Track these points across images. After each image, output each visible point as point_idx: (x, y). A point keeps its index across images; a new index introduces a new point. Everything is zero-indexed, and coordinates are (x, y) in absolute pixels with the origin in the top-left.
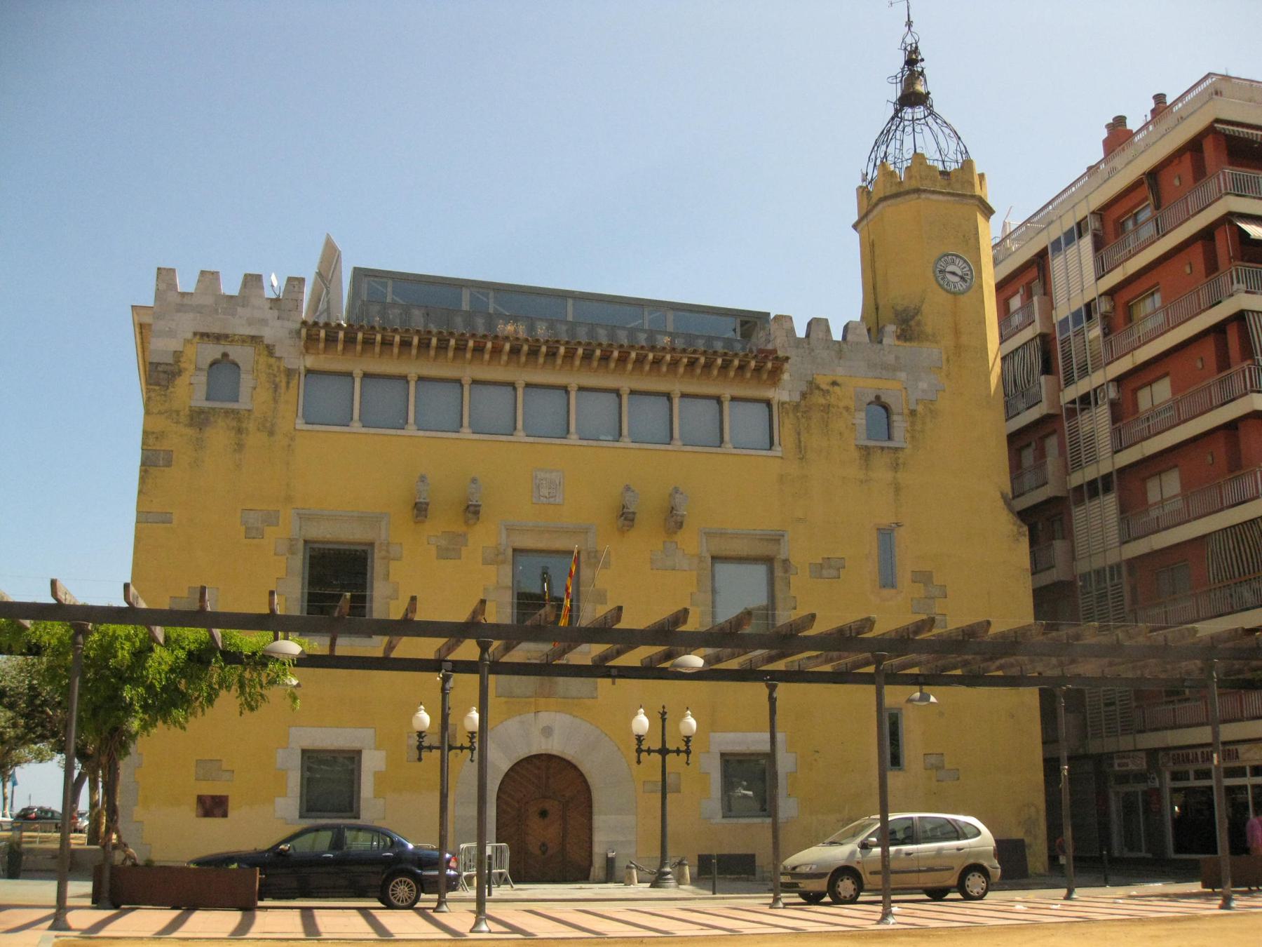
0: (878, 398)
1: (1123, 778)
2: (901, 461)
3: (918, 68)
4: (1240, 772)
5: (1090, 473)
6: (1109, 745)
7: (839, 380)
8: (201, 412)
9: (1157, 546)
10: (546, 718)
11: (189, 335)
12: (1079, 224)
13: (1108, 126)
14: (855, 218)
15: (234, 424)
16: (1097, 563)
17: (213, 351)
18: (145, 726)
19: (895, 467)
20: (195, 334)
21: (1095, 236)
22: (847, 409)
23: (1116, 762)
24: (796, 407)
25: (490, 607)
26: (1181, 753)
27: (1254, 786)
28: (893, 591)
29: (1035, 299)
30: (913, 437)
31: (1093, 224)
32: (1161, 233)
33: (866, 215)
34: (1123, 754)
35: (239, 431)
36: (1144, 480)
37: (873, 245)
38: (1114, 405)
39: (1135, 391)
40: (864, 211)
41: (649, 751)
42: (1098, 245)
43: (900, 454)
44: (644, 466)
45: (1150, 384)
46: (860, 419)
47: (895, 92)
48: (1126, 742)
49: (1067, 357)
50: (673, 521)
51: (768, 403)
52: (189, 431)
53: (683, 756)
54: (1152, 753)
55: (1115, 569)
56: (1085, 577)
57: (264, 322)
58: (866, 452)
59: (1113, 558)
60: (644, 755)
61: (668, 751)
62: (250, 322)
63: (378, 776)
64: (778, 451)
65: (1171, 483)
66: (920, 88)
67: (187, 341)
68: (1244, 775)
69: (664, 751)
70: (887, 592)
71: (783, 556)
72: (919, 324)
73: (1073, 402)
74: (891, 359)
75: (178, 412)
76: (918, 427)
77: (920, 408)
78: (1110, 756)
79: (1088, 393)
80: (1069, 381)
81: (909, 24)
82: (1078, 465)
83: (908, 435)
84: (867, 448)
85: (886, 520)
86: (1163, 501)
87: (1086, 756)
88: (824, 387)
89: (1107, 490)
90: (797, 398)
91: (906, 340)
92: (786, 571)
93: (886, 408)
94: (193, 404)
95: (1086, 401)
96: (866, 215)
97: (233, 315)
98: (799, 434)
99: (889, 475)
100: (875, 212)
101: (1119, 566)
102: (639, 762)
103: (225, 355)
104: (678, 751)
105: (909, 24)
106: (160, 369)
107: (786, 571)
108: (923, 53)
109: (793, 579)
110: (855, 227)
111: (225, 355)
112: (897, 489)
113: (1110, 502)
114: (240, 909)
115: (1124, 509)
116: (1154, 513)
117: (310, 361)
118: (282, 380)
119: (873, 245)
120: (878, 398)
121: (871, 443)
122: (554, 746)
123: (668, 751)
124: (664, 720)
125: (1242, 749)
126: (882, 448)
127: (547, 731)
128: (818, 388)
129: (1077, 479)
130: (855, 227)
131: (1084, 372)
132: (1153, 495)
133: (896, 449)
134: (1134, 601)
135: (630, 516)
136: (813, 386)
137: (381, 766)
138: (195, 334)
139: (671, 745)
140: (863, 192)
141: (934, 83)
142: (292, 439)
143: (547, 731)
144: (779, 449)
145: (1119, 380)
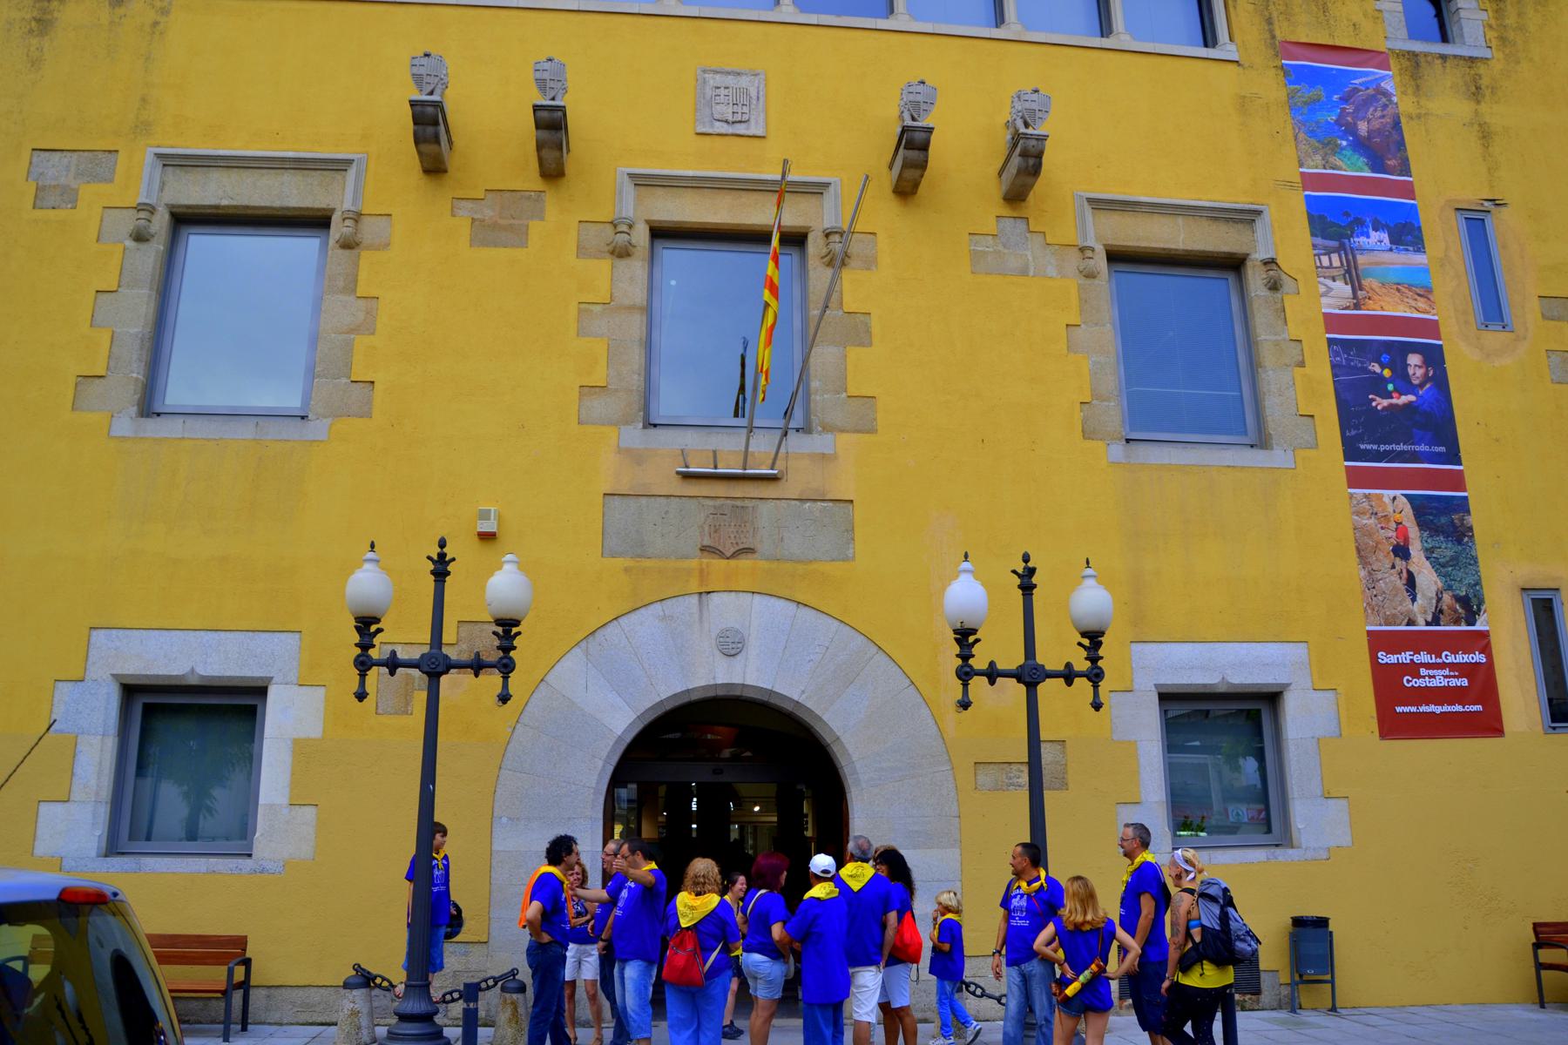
2: (1484, 82)
10: (727, 609)
18: (1128, 1007)
19: (1476, 92)
25: (695, 609)
28: (1503, 337)
30: (1502, 39)
41: (992, 674)
43: (1482, 69)
53: (1082, 684)
60: (978, 684)
63: (302, 750)
69: (1030, 676)
70: (1494, 338)
71: (1260, 254)
76: (1511, 20)
83: (1491, 34)
84: (1413, 56)
92: (1274, 286)
98: (1269, 21)
99: (1462, 108)
102: (965, 705)
104: (1069, 675)
107: (1274, 286)
109: (1290, 302)
114: (642, 959)
121: (1418, 47)
122: (752, 673)
124: (1027, 588)
126: (1444, 57)
127: (732, 646)
133: (1472, 59)
135: (919, 136)
137: (313, 728)
139: (1049, 657)
143: (732, 646)
144: (1233, 47)
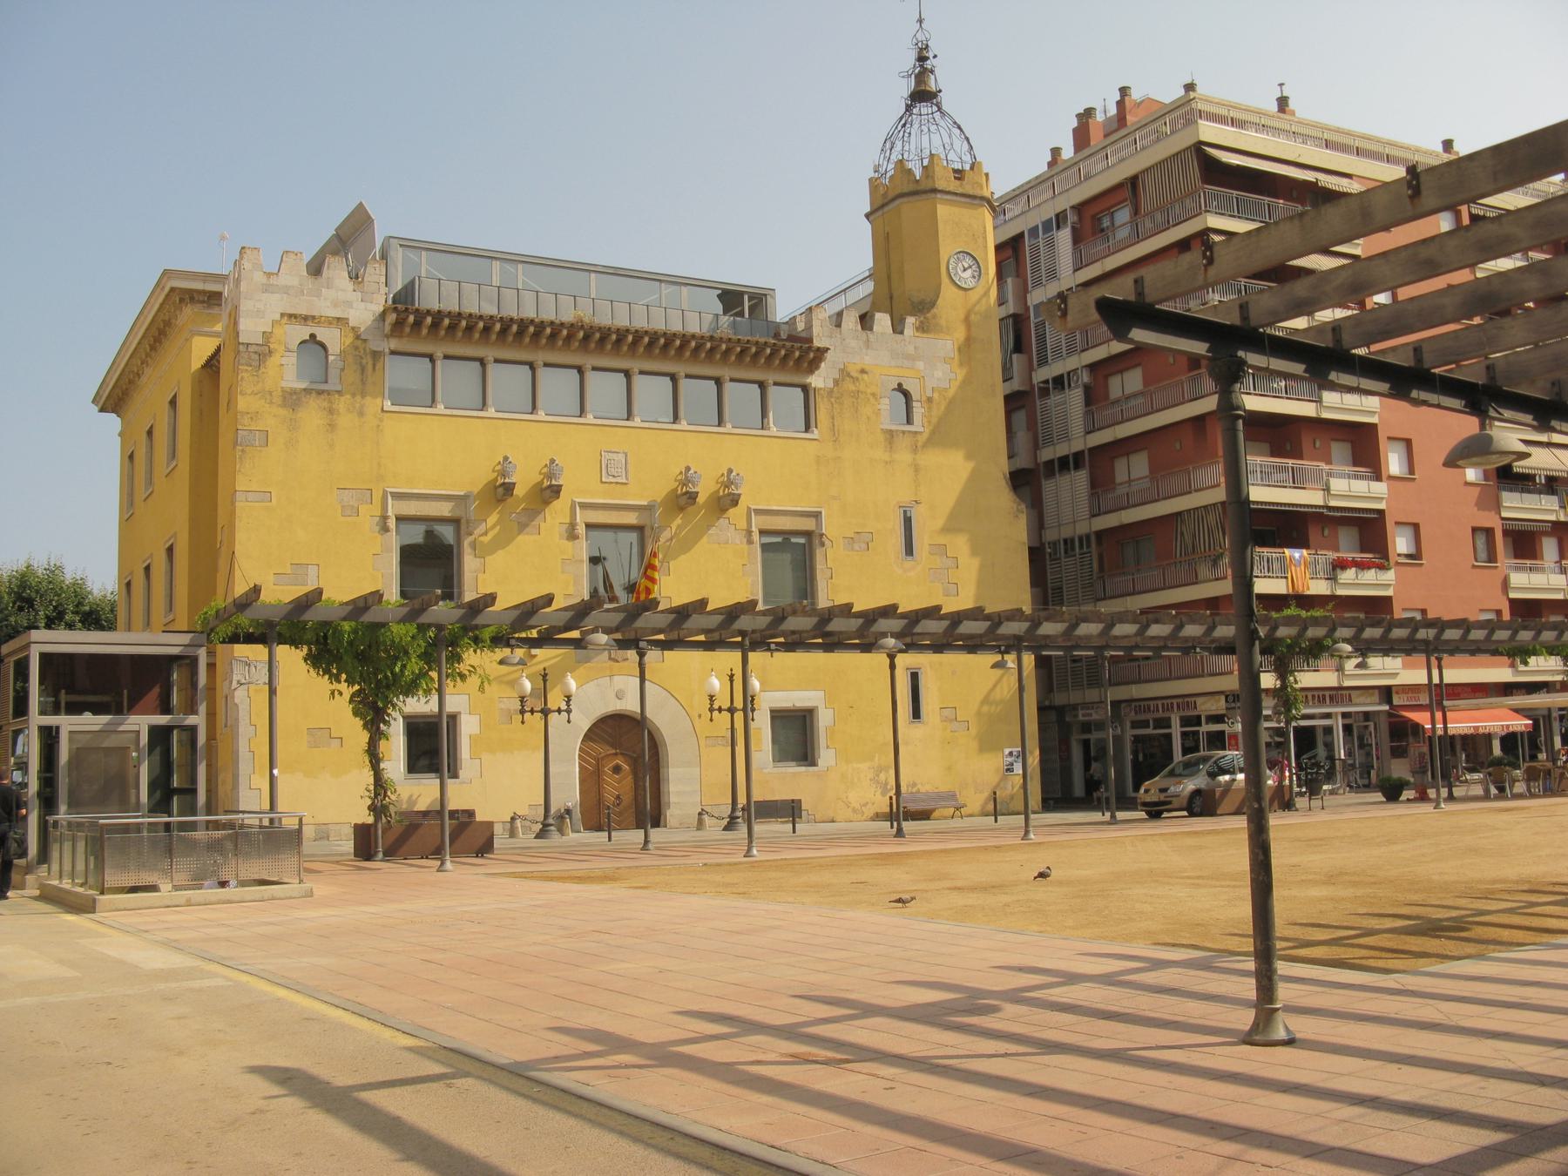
0: (900, 385)
1: (1087, 727)
3: (928, 65)
4: (1145, 724)
5: (1062, 450)
6: (1075, 697)
7: (867, 368)
8: (294, 392)
9: (1126, 521)
11: (277, 317)
12: (1057, 216)
13: (1078, 116)
14: (868, 209)
15: (325, 404)
16: (1066, 532)
17: (303, 332)
20: (282, 315)
21: (1074, 230)
22: (873, 395)
23: (1081, 712)
24: (831, 392)
26: (1186, 700)
27: (1169, 737)
29: (1009, 280)
31: (1072, 218)
32: (1138, 238)
33: (883, 206)
34: (1087, 705)
35: (331, 411)
36: (1113, 459)
37: (887, 237)
38: (1088, 390)
39: (1106, 377)
40: (879, 202)
42: (1077, 239)
44: (704, 452)
45: (1121, 372)
46: (885, 404)
47: (905, 87)
48: (1092, 695)
49: (1042, 339)
50: (726, 501)
51: (805, 389)
52: (283, 412)
54: (1116, 704)
55: (1085, 539)
56: (1054, 544)
57: (349, 304)
58: (890, 435)
59: (1082, 528)
61: (542, 711)
62: (335, 305)
64: (815, 434)
65: (1139, 465)
66: (932, 87)
67: (274, 323)
68: (1148, 726)
72: (934, 317)
73: (1046, 382)
74: (910, 349)
75: (270, 393)
77: (936, 396)
78: (1074, 707)
79: (1062, 376)
80: (1043, 361)
81: (920, 21)
82: (1049, 441)
85: (906, 497)
86: (1130, 481)
87: (1051, 708)
88: (854, 374)
89: (1077, 467)
90: (831, 384)
91: (924, 331)
93: (906, 394)
94: (284, 384)
95: (1059, 382)
96: (883, 206)
97: (319, 296)
100: (891, 206)
101: (1088, 536)
103: (313, 336)
105: (920, 21)
106: (251, 349)
108: (934, 48)
110: (867, 216)
111: (313, 336)
112: (917, 469)
113: (1081, 478)
115: (1094, 484)
116: (1121, 490)
117: (394, 344)
118: (368, 361)
119: (887, 237)
120: (900, 385)
121: (894, 428)
123: (542, 711)
125: (1199, 701)
128: (849, 375)
129: (1046, 454)
130: (867, 216)
131: (1058, 355)
132: (1121, 473)
134: (1101, 569)
136: (844, 373)
138: (282, 315)
140: (874, 185)
141: (941, 79)
142: (381, 420)
143: (619, 696)
145: (1093, 367)
